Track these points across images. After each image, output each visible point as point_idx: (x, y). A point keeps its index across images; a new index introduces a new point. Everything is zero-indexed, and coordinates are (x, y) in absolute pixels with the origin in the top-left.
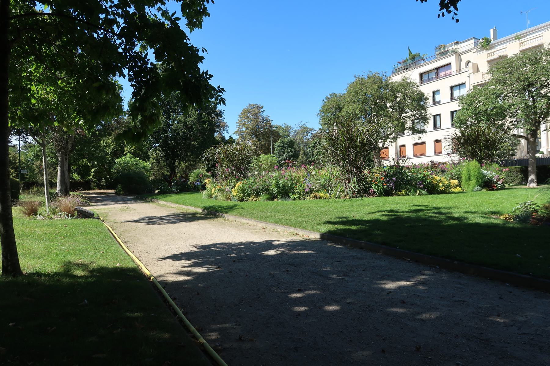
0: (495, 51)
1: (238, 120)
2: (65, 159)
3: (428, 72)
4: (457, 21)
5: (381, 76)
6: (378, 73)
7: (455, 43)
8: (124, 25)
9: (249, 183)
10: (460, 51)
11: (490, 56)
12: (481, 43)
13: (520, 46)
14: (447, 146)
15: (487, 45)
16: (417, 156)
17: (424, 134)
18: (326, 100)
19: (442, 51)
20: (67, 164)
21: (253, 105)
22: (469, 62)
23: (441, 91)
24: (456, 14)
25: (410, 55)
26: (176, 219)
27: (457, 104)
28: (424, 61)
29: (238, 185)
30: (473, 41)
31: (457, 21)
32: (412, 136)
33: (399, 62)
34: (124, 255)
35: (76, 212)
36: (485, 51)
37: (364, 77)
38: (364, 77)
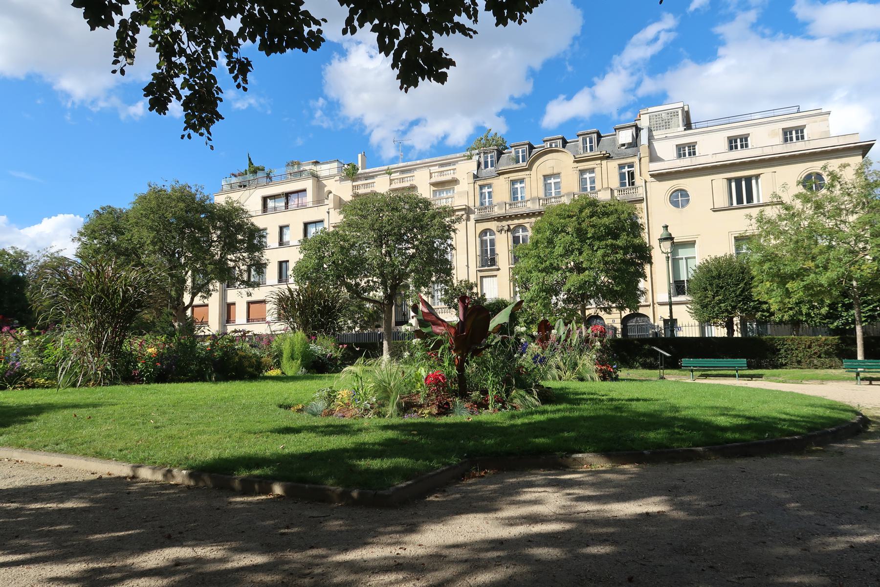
0: (405, 178)
3: (274, 197)
4: (212, 148)
5: (193, 191)
12: (346, 170)
13: (391, 184)
15: (352, 174)
16: (253, 320)
18: (93, 216)
22: (331, 192)
24: (210, 139)
28: (270, 179)
31: (212, 148)
32: (239, 290)
36: (350, 181)
37: (165, 187)
38: (165, 187)
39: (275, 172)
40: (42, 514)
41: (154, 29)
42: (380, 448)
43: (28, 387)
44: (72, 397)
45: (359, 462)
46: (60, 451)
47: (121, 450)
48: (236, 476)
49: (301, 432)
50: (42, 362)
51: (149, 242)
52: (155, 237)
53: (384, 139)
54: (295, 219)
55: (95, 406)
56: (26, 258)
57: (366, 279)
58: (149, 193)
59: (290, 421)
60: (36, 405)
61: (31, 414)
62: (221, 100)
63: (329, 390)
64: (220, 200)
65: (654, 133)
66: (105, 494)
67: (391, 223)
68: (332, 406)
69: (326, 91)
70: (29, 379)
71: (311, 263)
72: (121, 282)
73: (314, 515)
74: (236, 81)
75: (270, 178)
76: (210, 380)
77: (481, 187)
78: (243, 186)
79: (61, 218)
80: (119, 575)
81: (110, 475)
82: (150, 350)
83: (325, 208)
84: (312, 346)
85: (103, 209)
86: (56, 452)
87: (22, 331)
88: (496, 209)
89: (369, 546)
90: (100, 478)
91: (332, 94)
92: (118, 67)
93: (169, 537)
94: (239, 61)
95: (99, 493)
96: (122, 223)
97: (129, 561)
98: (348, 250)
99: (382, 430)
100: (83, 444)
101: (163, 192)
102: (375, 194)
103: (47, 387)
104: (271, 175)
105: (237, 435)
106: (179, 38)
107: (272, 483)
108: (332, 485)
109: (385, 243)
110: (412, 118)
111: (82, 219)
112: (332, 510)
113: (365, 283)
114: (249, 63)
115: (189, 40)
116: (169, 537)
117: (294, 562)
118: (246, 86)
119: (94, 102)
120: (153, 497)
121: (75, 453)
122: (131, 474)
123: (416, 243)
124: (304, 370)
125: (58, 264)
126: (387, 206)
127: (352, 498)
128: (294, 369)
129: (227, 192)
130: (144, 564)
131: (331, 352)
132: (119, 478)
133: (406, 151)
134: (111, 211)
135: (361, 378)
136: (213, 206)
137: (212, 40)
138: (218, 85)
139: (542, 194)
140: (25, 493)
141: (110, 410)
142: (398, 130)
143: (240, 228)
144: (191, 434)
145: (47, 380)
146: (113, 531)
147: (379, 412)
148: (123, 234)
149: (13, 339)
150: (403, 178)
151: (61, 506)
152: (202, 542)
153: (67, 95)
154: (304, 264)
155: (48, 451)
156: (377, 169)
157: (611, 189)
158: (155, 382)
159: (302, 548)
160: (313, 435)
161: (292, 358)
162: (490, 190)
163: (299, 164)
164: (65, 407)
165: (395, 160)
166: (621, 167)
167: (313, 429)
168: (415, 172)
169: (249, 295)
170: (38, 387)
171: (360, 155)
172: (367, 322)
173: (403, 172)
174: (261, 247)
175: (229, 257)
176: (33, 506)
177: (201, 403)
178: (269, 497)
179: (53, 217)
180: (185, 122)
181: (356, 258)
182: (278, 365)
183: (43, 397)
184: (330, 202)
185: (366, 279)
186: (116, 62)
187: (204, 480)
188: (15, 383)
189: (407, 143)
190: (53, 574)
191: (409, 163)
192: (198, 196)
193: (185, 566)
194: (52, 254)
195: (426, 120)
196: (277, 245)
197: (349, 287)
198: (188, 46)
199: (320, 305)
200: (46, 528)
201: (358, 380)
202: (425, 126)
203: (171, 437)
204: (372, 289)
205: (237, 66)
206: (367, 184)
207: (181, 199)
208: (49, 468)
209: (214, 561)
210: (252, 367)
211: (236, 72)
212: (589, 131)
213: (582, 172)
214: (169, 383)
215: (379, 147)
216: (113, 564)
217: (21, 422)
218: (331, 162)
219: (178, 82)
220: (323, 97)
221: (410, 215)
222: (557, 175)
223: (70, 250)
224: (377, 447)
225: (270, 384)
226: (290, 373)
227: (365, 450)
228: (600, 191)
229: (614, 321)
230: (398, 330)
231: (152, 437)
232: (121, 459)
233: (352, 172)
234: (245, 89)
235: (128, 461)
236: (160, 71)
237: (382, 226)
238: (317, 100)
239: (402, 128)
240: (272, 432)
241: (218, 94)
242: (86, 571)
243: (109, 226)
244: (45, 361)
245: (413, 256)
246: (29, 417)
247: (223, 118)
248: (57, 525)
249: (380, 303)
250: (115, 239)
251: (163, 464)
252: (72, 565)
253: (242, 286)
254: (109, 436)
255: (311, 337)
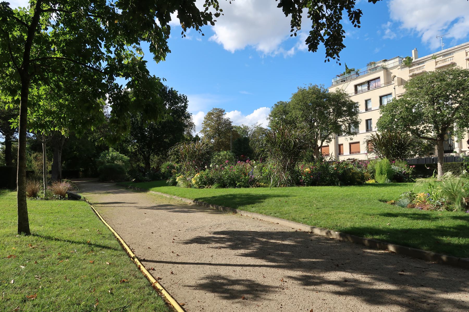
1: (204, 121)
2: (59, 153)
3: (361, 84)
4: (340, 64)
5: (319, 88)
6: (317, 86)
7: (383, 61)
8: (108, 66)
9: (207, 173)
10: (389, 67)
11: (445, 62)
12: (404, 61)
13: (436, 65)
14: (363, 148)
15: (408, 63)
16: (353, 153)
17: (355, 136)
18: (274, 107)
19: (373, 67)
20: (61, 156)
21: (216, 109)
22: (395, 76)
23: (372, 100)
24: (338, 60)
25: (346, 70)
26: (325, 243)
27: (379, 112)
28: (358, 75)
29: (198, 175)
30: (397, 59)
32: (346, 137)
33: (338, 75)
34: (102, 225)
35: (67, 195)
36: (407, 68)
39: (361, 70)
40: (277, 245)
41: (310, 8)
42: (455, 231)
43: (258, 187)
44: (276, 192)
45: (442, 238)
46: (277, 217)
47: (304, 219)
48: (365, 238)
49: (398, 217)
50: (261, 175)
51: (300, 116)
52: (302, 114)
53: (431, 38)
54: (374, 95)
55: (287, 196)
56: (248, 129)
57: (423, 126)
58: (298, 92)
59: (389, 210)
60: (263, 195)
61: (262, 199)
62: (344, 37)
63: (410, 193)
64: (332, 90)
66: (301, 239)
67: (441, 89)
68: (414, 202)
69: (391, 17)
70: (258, 183)
71: (387, 119)
72: (293, 137)
73: (418, 266)
74: (353, 24)
75: (358, 74)
76: (338, 185)
78: (343, 81)
79: (261, 109)
80: (318, 281)
81: (300, 230)
82: (307, 170)
83: (393, 86)
84: (393, 167)
85: (278, 103)
86: (275, 217)
87: (253, 162)
89: (463, 292)
90: (296, 231)
91: (395, 18)
92: (293, 33)
93: (338, 266)
94: (355, 12)
95: (298, 238)
96: (287, 109)
97: (321, 275)
98: (411, 109)
99: (453, 219)
100: (286, 214)
101: (305, 91)
102: (424, 73)
103: (265, 187)
104: (359, 72)
105: (361, 215)
106: (322, 9)
107: (387, 244)
108: (426, 250)
109: (436, 102)
110: (452, 19)
111: (270, 109)
112: (429, 265)
113: (423, 128)
114: (360, 12)
115: (327, 9)
116: (338, 266)
117: (413, 293)
118: (359, 25)
119: (273, 53)
120: (323, 244)
121: (284, 218)
122: (310, 231)
123: (460, 99)
124: (389, 180)
125: (261, 130)
126: (437, 78)
127: (442, 260)
128: (383, 180)
129: (335, 86)
130: (329, 278)
131: (404, 170)
132: (305, 232)
133: (448, 42)
134: (282, 103)
135: (433, 186)
136: (329, 94)
137: (338, 5)
138: (343, 29)
140: (267, 235)
141: (294, 198)
142: (443, 30)
143: (344, 104)
144: (336, 213)
145: (264, 184)
146: (309, 258)
147: (447, 208)
148: (288, 114)
149: (250, 165)
150: (445, 60)
151: (284, 243)
152: (355, 271)
153: (262, 52)
154: (382, 119)
155: (272, 216)
156: (426, 57)
158: (311, 185)
159: (416, 286)
160: (405, 218)
161: (381, 173)
163: (374, 63)
164: (275, 196)
165: (439, 49)
167: (405, 215)
168: (454, 54)
169: (351, 139)
170: (261, 187)
171: (413, 51)
172: (424, 151)
173: (444, 55)
174: (356, 113)
175: (338, 120)
176: (272, 241)
177: (336, 197)
178: (386, 252)
179: (258, 109)
180: (326, 53)
181: (416, 113)
182: (373, 177)
183: (264, 191)
184: (395, 82)
185: (423, 126)
186: (292, 31)
187: (347, 238)
188: (253, 185)
189: (448, 36)
190: (289, 275)
191: (449, 49)
192: (322, 90)
193: (350, 283)
194: (257, 126)
195: (463, 18)
196: (364, 111)
197: (413, 132)
198: (327, 12)
199: (396, 143)
200: (280, 252)
201: (431, 188)
202: (463, 22)
203: (326, 214)
204: (428, 131)
205: (354, 15)
206: (419, 67)
207: (313, 93)
208: (273, 224)
209: (365, 283)
210: (359, 178)
211: (353, 19)
214: (317, 186)
215: (429, 43)
216: (314, 275)
217: (260, 202)
218: (394, 59)
219: (322, 32)
220: (390, 21)
221: (454, 82)
223: (265, 124)
224: (452, 230)
225: (371, 188)
226: (381, 182)
227: (446, 231)
230: (446, 156)
231: (317, 213)
232: (304, 223)
233: (408, 62)
234: (359, 27)
235: (308, 224)
236: (313, 29)
237: (434, 92)
238: (387, 24)
239: (445, 28)
240: (381, 215)
241: (342, 34)
242: (303, 276)
243: (282, 111)
244: (263, 175)
245: (457, 108)
246: (262, 200)
247: (345, 47)
248: (284, 251)
249: (434, 139)
250: (284, 117)
251: (325, 227)
252: (296, 272)
253: (347, 135)
254: (296, 211)
255: (392, 161)
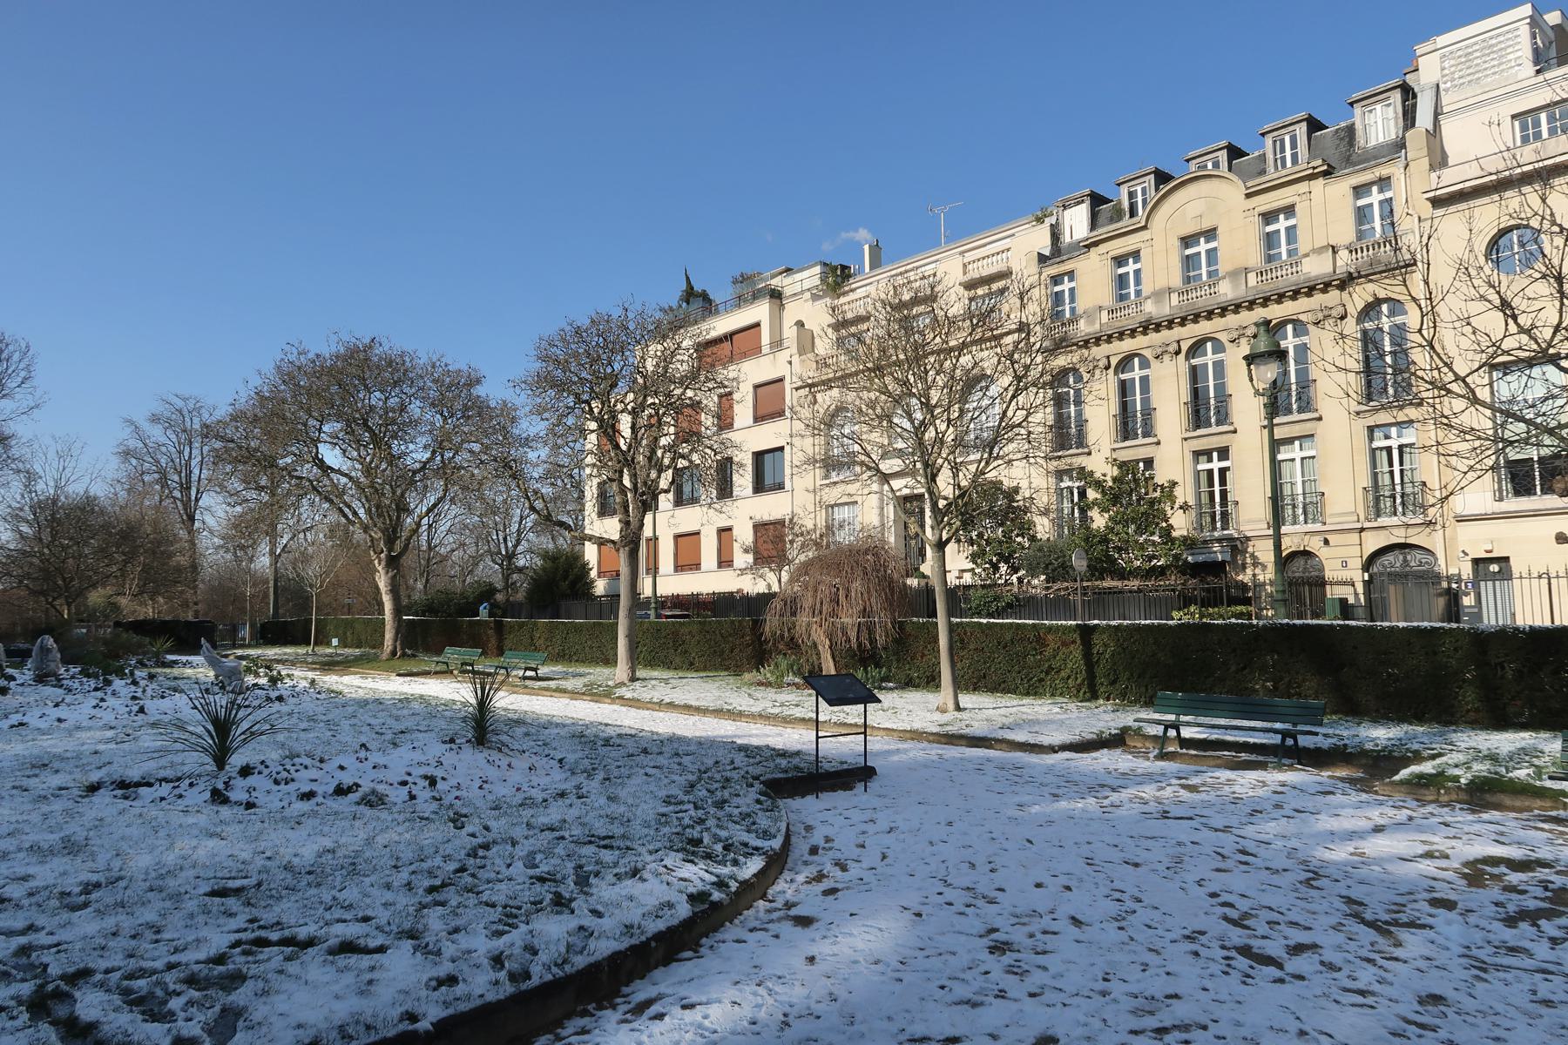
65: (1445, 100)
77: (1056, 280)
88: (1082, 323)
139: (1176, 280)
157: (1333, 247)
162: (1292, 222)
166: (1359, 191)
212: (1289, 119)
213: (1269, 217)
222: (1210, 234)
228: (1307, 255)
229: (1345, 565)
